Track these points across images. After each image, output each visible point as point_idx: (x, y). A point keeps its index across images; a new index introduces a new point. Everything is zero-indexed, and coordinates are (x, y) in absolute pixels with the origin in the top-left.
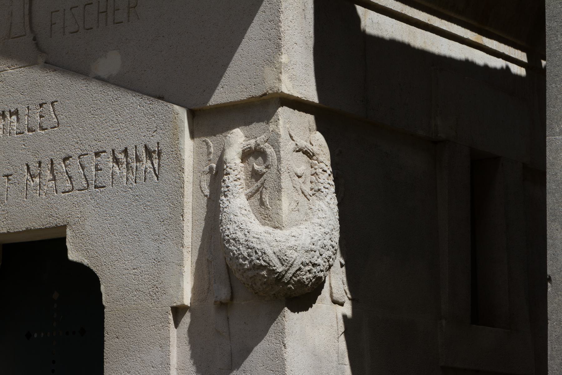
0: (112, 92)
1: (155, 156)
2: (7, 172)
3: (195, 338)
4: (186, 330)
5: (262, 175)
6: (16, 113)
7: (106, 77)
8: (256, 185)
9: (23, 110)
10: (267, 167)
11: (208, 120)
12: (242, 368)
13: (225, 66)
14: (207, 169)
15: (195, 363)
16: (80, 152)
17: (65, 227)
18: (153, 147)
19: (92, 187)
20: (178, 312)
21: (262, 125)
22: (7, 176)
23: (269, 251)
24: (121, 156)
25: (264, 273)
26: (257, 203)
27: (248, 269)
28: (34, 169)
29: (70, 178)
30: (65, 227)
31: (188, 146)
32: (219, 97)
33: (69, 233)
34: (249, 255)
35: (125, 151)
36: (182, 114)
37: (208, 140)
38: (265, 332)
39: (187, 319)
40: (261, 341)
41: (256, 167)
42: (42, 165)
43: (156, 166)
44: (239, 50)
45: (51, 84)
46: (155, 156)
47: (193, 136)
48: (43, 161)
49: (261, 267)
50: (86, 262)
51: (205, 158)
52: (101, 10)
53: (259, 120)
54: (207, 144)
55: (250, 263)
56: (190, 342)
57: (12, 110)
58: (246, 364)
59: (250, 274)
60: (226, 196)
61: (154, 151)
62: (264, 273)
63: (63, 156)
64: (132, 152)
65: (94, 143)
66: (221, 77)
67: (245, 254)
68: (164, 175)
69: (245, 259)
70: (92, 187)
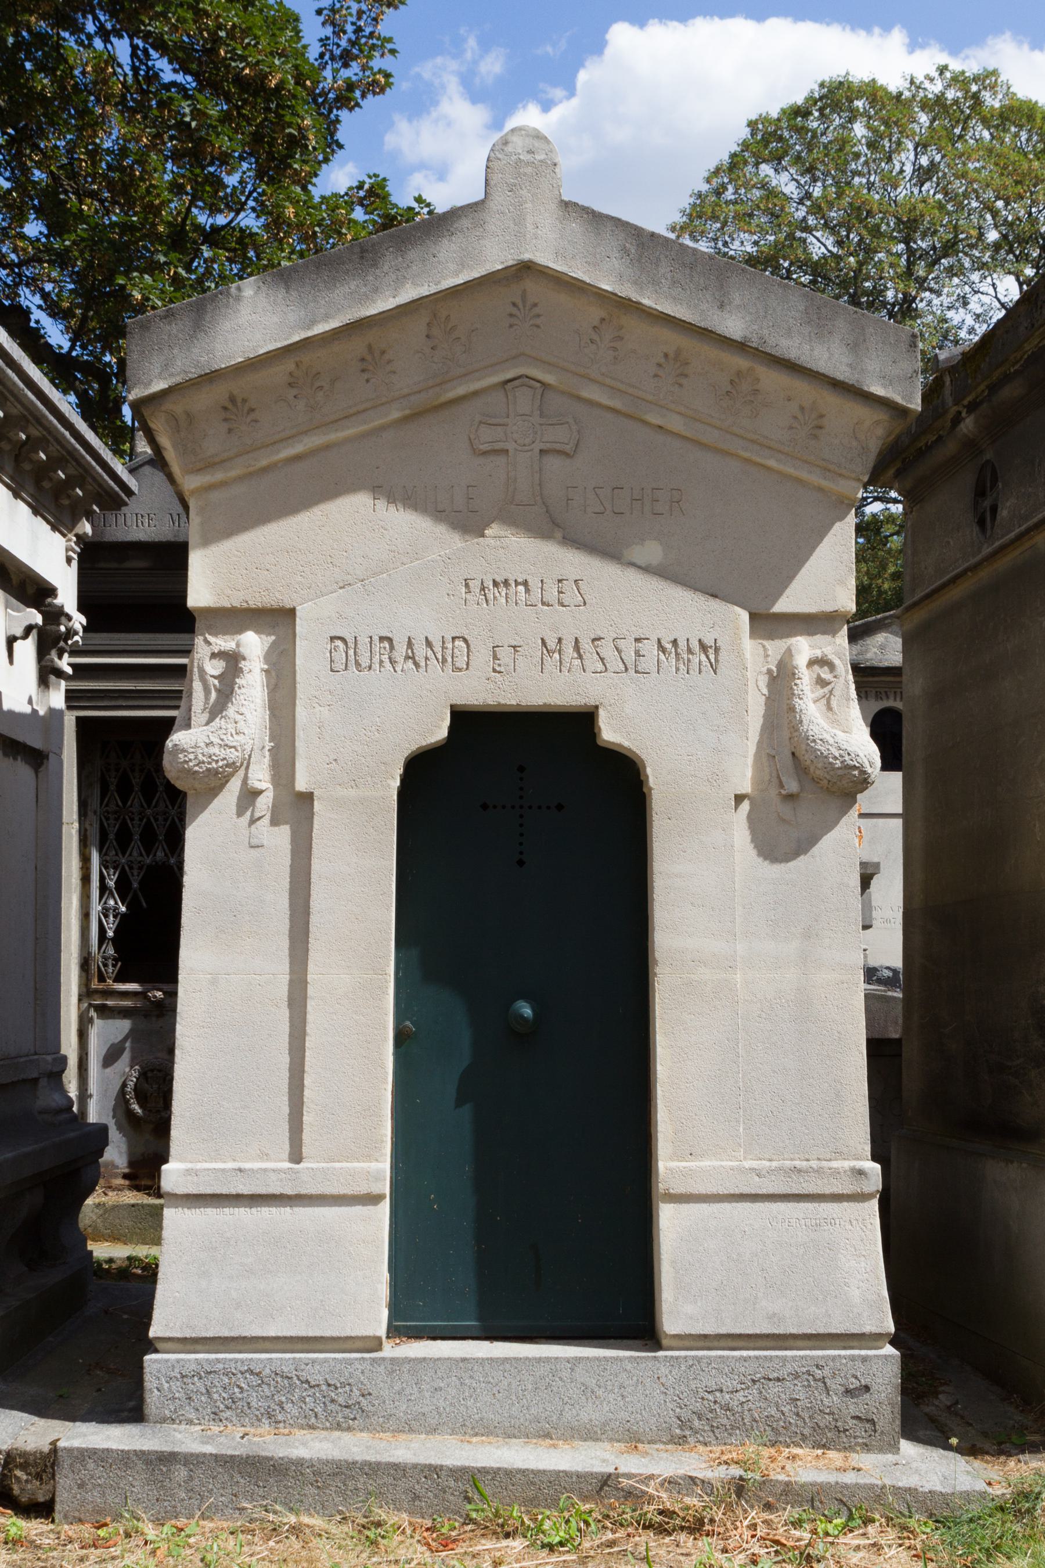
0: (654, 584)
1: (711, 651)
2: (514, 643)
3: (753, 820)
4: (745, 816)
5: (830, 683)
6: (525, 583)
7: (643, 565)
8: (821, 692)
9: (534, 584)
10: (835, 677)
11: (767, 623)
12: (810, 853)
13: (791, 578)
14: (764, 670)
15: (755, 847)
16: (615, 636)
17: (597, 707)
18: (709, 641)
19: (632, 672)
20: (739, 799)
21: (828, 638)
22: (514, 647)
23: (861, 755)
24: (669, 646)
25: (856, 773)
26: (824, 708)
27: (838, 768)
28: (552, 644)
29: (602, 659)
30: (597, 707)
31: (749, 646)
32: (782, 606)
33: (602, 714)
34: (841, 756)
35: (675, 642)
36: (744, 616)
37: (765, 643)
38: (836, 822)
39: (746, 806)
40: (830, 830)
41: (823, 676)
42: (564, 642)
43: (713, 660)
44: (807, 565)
45: (573, 562)
46: (711, 651)
47: (751, 637)
48: (564, 637)
49: (855, 767)
50: (626, 744)
51: (762, 659)
52: (635, 497)
53: (824, 633)
54: (764, 646)
55: (842, 762)
56: (749, 828)
57: (519, 580)
58: (815, 850)
59: (840, 772)
60: (801, 699)
61: (711, 647)
62: (856, 773)
63: (593, 637)
64: (682, 644)
65: (634, 628)
66: (786, 587)
67: (837, 755)
68: (722, 668)
69: (835, 758)
70: (632, 672)
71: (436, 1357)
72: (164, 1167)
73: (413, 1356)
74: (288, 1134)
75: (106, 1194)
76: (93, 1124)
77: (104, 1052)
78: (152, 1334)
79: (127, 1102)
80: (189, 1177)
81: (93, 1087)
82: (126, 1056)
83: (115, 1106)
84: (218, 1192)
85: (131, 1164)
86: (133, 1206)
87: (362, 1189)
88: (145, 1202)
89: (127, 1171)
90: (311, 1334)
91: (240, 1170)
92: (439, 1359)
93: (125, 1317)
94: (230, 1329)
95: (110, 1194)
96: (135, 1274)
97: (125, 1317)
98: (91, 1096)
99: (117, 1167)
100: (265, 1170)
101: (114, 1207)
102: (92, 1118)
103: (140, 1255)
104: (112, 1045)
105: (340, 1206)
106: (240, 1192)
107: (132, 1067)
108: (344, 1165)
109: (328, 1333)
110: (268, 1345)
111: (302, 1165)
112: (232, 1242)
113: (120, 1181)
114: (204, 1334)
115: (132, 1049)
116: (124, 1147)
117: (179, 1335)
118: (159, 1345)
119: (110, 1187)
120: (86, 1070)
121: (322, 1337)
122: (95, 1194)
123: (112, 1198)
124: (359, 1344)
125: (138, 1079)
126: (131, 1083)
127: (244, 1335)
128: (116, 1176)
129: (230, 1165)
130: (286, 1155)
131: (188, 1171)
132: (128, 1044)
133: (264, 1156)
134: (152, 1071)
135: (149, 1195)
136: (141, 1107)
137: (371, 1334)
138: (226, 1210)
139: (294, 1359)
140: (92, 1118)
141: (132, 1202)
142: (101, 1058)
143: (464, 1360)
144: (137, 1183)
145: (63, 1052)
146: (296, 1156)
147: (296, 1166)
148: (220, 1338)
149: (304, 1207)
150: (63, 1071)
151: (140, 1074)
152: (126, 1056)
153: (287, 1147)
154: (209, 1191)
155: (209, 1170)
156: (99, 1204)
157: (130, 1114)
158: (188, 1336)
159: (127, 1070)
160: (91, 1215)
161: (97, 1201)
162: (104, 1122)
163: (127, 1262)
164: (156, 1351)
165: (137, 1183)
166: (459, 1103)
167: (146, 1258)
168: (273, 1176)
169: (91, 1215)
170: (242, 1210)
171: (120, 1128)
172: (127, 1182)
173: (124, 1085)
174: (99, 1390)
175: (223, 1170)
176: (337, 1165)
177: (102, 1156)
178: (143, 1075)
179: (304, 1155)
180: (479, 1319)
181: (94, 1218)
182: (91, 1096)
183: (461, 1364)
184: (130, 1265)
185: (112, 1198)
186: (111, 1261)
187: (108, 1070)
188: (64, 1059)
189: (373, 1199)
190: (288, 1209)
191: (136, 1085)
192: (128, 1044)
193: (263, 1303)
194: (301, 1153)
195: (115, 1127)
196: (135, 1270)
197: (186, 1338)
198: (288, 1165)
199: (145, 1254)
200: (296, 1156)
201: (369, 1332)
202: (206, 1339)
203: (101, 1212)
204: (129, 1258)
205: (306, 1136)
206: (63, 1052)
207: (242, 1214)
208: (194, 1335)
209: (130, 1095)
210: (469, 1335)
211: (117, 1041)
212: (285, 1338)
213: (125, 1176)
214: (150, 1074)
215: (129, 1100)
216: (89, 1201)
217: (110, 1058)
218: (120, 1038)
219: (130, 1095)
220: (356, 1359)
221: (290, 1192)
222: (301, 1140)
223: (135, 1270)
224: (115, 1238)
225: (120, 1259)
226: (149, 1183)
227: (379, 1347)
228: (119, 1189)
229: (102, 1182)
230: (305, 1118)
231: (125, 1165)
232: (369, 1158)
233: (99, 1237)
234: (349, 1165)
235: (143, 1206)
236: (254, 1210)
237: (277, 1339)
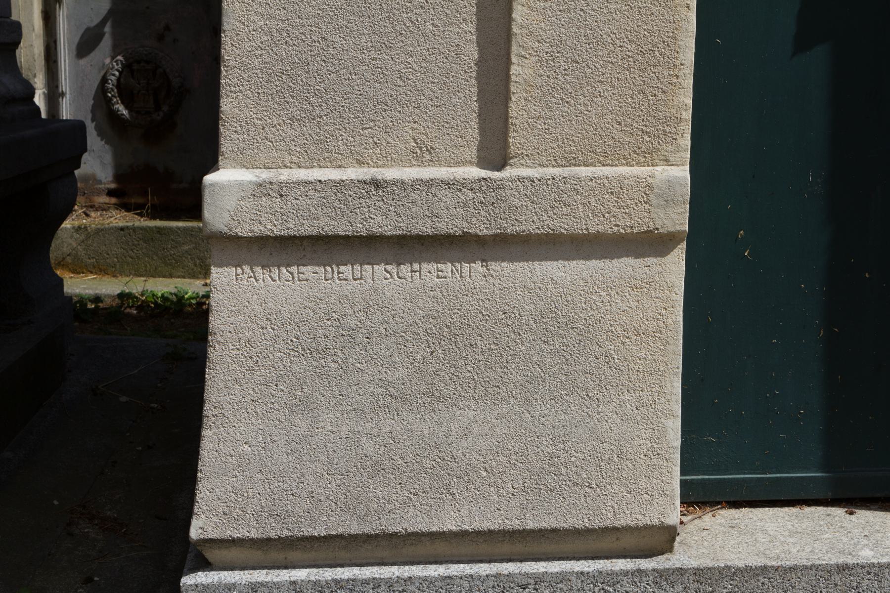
71: (789, 563)
72: (210, 178)
73: (741, 564)
74: (475, 106)
75: (87, 215)
76: (66, 120)
77: (77, 40)
78: (194, 533)
79: (109, 101)
80: (264, 201)
81: (65, 83)
82: (107, 43)
83: (93, 106)
84: (329, 231)
85: (117, 178)
86: (122, 229)
87: (636, 221)
88: (137, 224)
89: (113, 186)
90: (531, 525)
91: (376, 183)
92: (793, 569)
93: (123, 399)
94: (362, 519)
95: (93, 214)
96: (129, 315)
97: (123, 399)
98: (63, 94)
99: (100, 182)
100: (430, 183)
101: (98, 231)
102: (66, 112)
103: (134, 291)
104: (88, 30)
105: (588, 258)
106: (377, 231)
107: (113, 58)
108: (600, 171)
109: (566, 522)
110: (440, 548)
111: (508, 173)
112: (360, 337)
113: (104, 199)
114: (308, 531)
115: (114, 35)
116: (108, 158)
117: (254, 534)
118: (211, 555)
119: (92, 207)
120: (56, 62)
121: (554, 531)
122: (74, 215)
123: (95, 220)
124: (628, 542)
125: (120, 73)
126: (113, 78)
127: (391, 529)
128: (99, 193)
129: (352, 173)
130: (472, 152)
131: (262, 189)
132: (107, 29)
133: (424, 153)
134: (138, 62)
135: (141, 215)
136: (127, 107)
137: (656, 522)
138: (346, 269)
139: (498, 576)
140: (66, 112)
141: (121, 224)
142: (74, 47)
143: (842, 568)
144: (126, 200)
145: (14, 17)
146: (495, 152)
147: (496, 175)
148: (341, 537)
149: (511, 260)
150: (17, 44)
151: (124, 66)
152: (107, 43)
153: (473, 132)
154: (308, 229)
155: (306, 183)
156: (79, 228)
157: (113, 116)
158: (272, 535)
159: (108, 61)
160: (70, 241)
161: (76, 223)
162: (79, 118)
163: (117, 301)
164: (205, 565)
165: (126, 200)
166: (802, 43)
167: (142, 295)
168: (447, 197)
169: (70, 241)
170: (380, 268)
171: (101, 133)
172: (114, 200)
173: (104, 80)
174: (89, 580)
175: (339, 184)
176: (584, 171)
177: (78, 166)
178: (127, 68)
179: (513, 149)
180: (826, 466)
181: (74, 244)
182: (63, 94)
183: (837, 578)
184: (123, 304)
185: (95, 220)
186: (97, 299)
187: (83, 62)
188: (16, 29)
189: (653, 243)
190: (478, 266)
191: (118, 80)
192: (107, 29)
193: (428, 464)
194: (506, 145)
195: (95, 133)
196: (128, 310)
197: (269, 540)
198: (475, 172)
199: (140, 289)
200: (495, 152)
201: (650, 518)
202: (311, 539)
203: (82, 237)
204: (122, 296)
205: (518, 109)
206: (14, 17)
207: (381, 278)
208: (285, 533)
209: (112, 93)
210: (803, 496)
211: (93, 24)
212: (478, 533)
213: (110, 193)
214: (135, 67)
215: (111, 99)
216: (67, 224)
217: (86, 45)
218: (96, 21)
219: (112, 93)
220: (626, 573)
221: (483, 230)
222: (506, 117)
223: (128, 310)
224: (102, 269)
225: (109, 296)
226: (140, 200)
227: (663, 539)
228: (103, 208)
229: (80, 199)
230: (514, 69)
231: (110, 178)
232: (650, 156)
233: (78, 268)
234: (608, 171)
235: (134, 229)
236: (405, 269)
237: (461, 535)
